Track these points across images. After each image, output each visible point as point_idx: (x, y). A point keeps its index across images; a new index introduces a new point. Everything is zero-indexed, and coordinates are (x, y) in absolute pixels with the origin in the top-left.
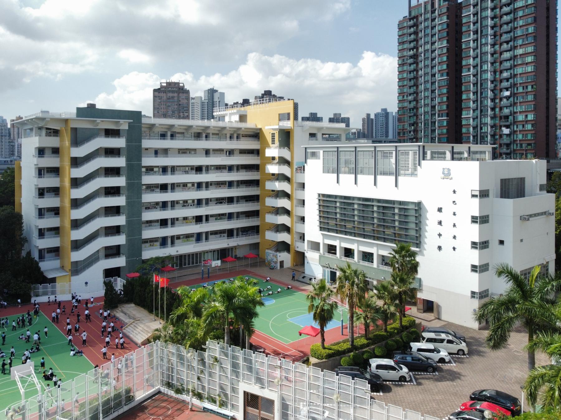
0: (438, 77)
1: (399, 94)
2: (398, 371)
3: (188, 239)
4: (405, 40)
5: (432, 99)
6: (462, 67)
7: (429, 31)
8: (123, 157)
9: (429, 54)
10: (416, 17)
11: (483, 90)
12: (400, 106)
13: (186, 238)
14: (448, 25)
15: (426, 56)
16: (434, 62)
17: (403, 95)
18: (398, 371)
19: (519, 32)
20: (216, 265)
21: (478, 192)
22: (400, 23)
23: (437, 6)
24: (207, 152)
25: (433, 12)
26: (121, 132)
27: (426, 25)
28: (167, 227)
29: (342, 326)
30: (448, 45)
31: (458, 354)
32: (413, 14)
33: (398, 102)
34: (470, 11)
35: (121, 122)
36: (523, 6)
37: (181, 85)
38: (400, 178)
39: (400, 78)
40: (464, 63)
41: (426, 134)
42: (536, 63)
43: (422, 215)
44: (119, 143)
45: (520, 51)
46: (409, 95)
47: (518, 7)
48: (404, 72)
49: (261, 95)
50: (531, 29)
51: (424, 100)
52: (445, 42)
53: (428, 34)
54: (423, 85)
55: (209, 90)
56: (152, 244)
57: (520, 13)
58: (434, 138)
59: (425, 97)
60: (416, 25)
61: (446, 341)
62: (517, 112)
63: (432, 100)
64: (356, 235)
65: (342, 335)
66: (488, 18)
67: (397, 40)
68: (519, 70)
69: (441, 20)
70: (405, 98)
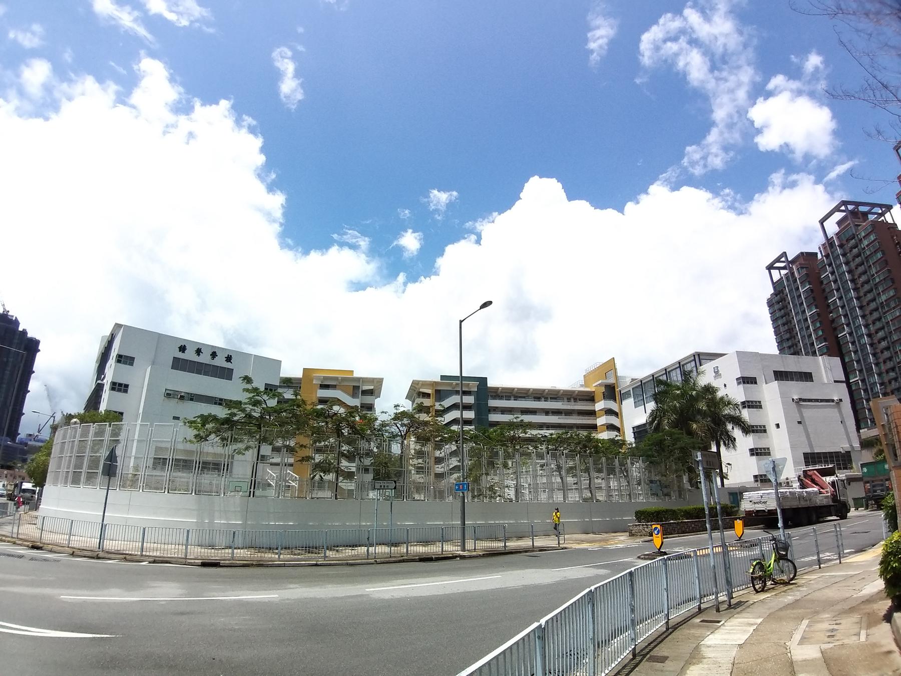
32: (778, 289)
44: (469, 400)
45: (884, 298)
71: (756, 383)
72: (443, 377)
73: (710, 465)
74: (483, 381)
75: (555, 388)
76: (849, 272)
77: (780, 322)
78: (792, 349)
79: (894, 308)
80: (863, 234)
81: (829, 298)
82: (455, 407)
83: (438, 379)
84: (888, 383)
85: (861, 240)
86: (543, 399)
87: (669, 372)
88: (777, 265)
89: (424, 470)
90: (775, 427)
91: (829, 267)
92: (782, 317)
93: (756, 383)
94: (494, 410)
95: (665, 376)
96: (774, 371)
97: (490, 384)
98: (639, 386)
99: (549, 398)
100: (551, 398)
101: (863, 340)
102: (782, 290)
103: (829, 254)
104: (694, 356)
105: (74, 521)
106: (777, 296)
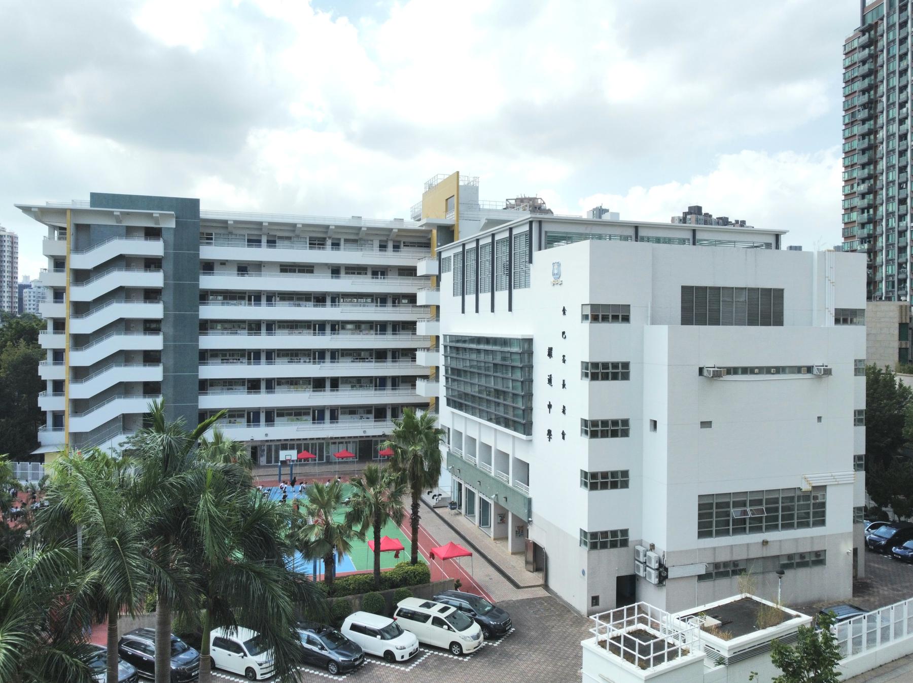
1: (845, 181)
2: (245, 655)
3: (299, 417)
4: (856, 74)
5: (900, 184)
9: (896, 97)
10: (874, 27)
12: (846, 206)
13: (295, 415)
15: (891, 101)
16: (904, 110)
17: (851, 183)
18: (245, 655)
20: (288, 458)
21: (589, 307)
22: (849, 41)
24: (335, 271)
26: (163, 232)
27: (891, 38)
28: (259, 392)
31: (450, 651)
32: (870, 20)
33: (843, 198)
37: (539, 201)
38: (514, 292)
39: (847, 150)
43: (534, 367)
46: (860, 181)
48: (853, 138)
49: (681, 215)
51: (887, 190)
55: (594, 210)
56: (232, 420)
58: (904, 265)
59: (888, 183)
60: (872, 42)
61: (431, 620)
63: (900, 188)
64: (485, 414)
67: (842, 77)
70: (855, 189)
71: (626, 319)
72: (96, 198)
82: (123, 262)
90: (647, 426)
93: (626, 319)
100: (346, 241)
106: (864, 35)
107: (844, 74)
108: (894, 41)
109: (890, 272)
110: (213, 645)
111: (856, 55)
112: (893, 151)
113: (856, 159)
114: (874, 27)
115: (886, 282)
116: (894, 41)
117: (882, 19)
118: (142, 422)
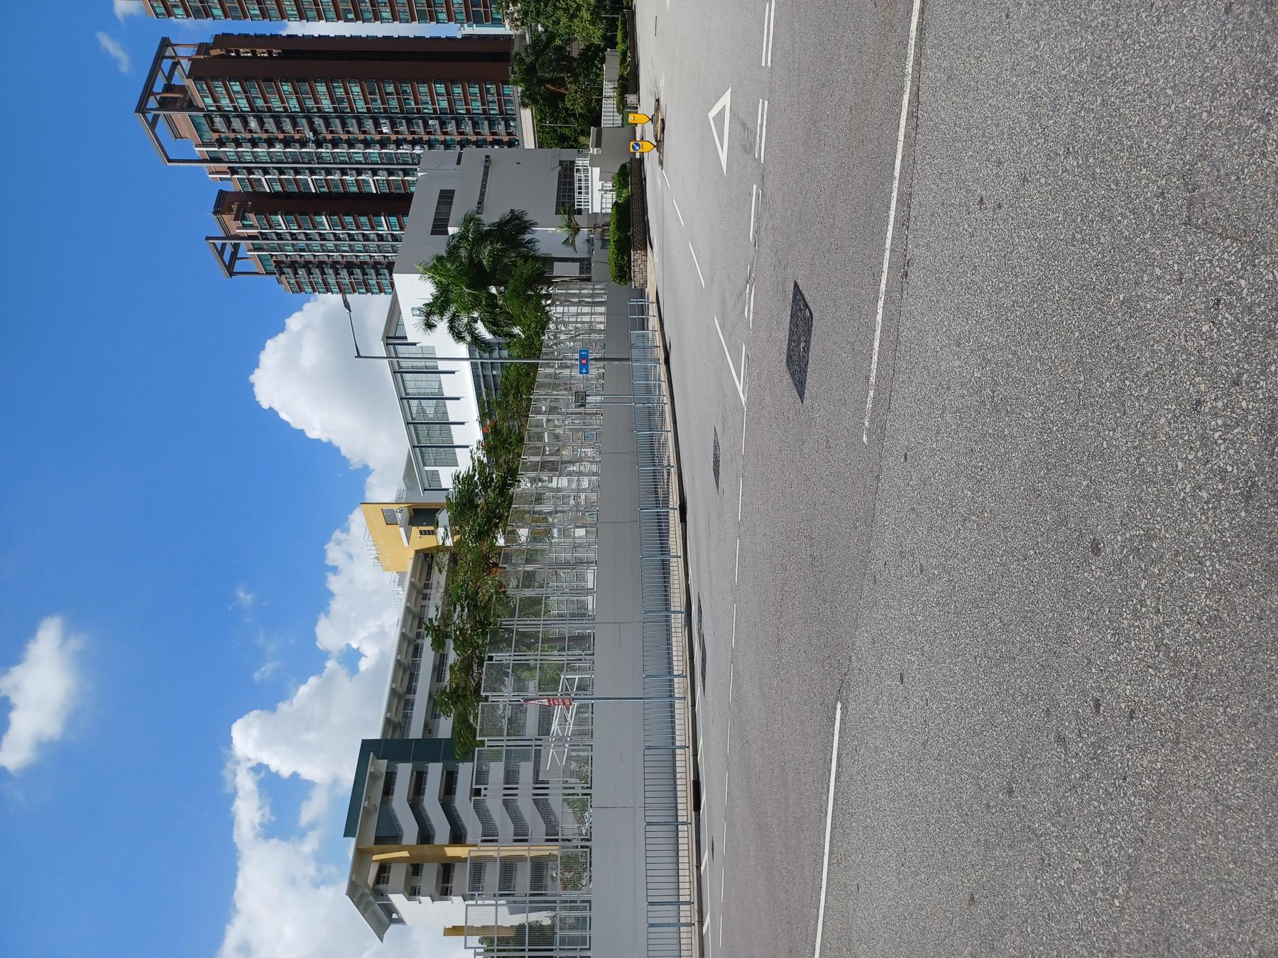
0: (384, 230)
6: (361, 192)
7: (330, 245)
8: (458, 767)
10: (279, 264)
11: (274, 160)
14: (332, 214)
19: (243, 104)
23: (254, 232)
25: (264, 237)
29: (387, 358)
30: (280, 212)
32: (272, 268)
34: (260, 179)
35: (372, 771)
36: (247, 98)
40: (354, 189)
41: (390, 249)
42: (345, 78)
44: (404, 771)
45: (326, 104)
47: (247, 106)
50: (287, 88)
52: (318, 219)
53: (364, 246)
54: (373, 254)
57: (260, 103)
62: (435, 110)
65: (359, 356)
66: (239, 152)
68: (360, 105)
69: (323, 225)
72: (349, 832)
73: (588, 205)
74: (368, 747)
75: (400, 622)
76: (271, 145)
77: (331, 280)
78: (382, 271)
79: (347, 93)
80: (209, 101)
81: (307, 191)
83: (352, 841)
84: (463, 137)
85: (219, 109)
86: (410, 697)
87: (407, 394)
88: (227, 257)
89: (527, 947)
91: (253, 174)
92: (323, 273)
94: (430, 733)
95: (411, 401)
96: (431, 234)
97: (376, 734)
98: (420, 451)
99: (419, 630)
101: (372, 235)
102: (275, 261)
103: (229, 168)
104: (387, 344)
105: (651, 921)
107: (319, 292)
108: (293, 245)
109: (290, 248)
110: (480, 796)
111: (329, 280)
112: (393, 246)
113: (373, 282)
114: (279, 264)
115: (272, 251)
116: (293, 245)
117: (272, 256)
118: (527, 822)
